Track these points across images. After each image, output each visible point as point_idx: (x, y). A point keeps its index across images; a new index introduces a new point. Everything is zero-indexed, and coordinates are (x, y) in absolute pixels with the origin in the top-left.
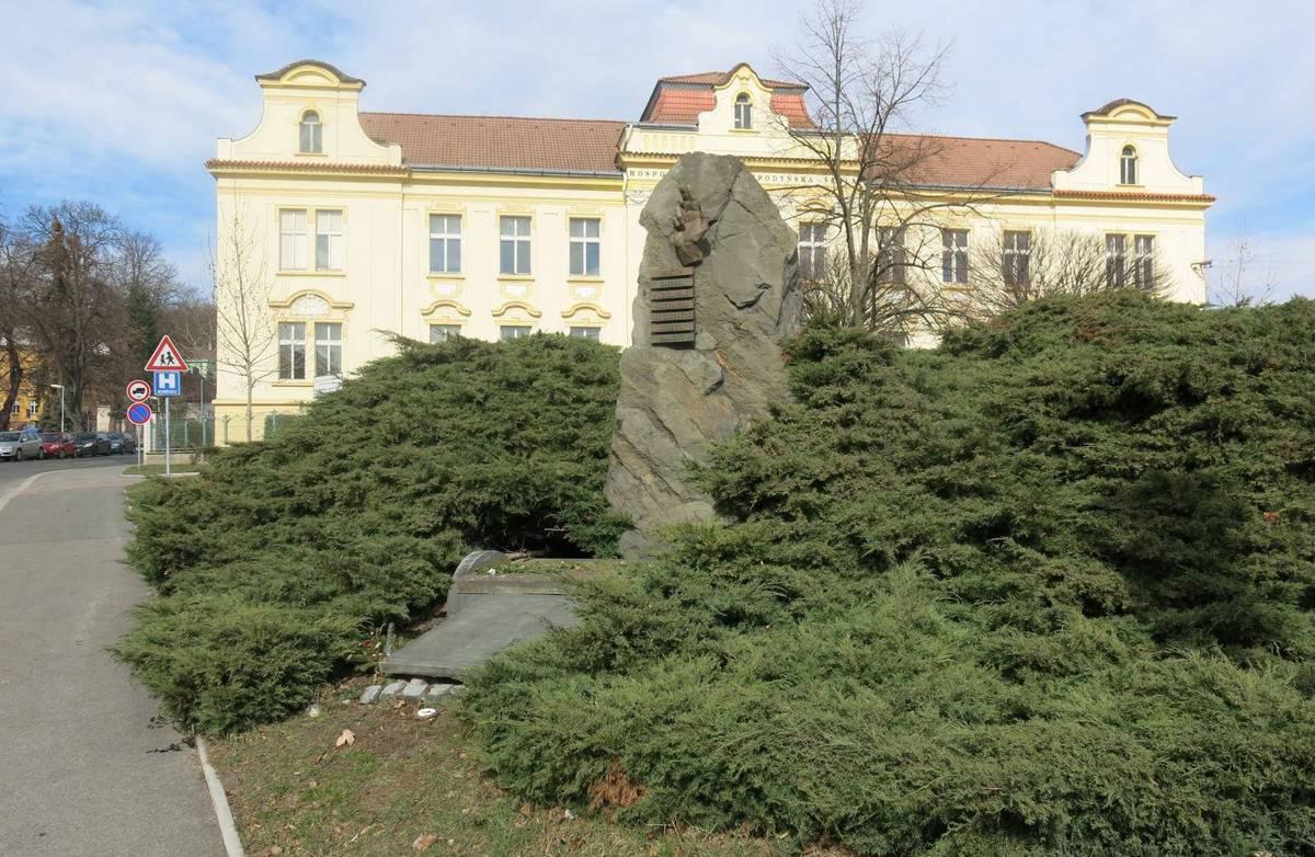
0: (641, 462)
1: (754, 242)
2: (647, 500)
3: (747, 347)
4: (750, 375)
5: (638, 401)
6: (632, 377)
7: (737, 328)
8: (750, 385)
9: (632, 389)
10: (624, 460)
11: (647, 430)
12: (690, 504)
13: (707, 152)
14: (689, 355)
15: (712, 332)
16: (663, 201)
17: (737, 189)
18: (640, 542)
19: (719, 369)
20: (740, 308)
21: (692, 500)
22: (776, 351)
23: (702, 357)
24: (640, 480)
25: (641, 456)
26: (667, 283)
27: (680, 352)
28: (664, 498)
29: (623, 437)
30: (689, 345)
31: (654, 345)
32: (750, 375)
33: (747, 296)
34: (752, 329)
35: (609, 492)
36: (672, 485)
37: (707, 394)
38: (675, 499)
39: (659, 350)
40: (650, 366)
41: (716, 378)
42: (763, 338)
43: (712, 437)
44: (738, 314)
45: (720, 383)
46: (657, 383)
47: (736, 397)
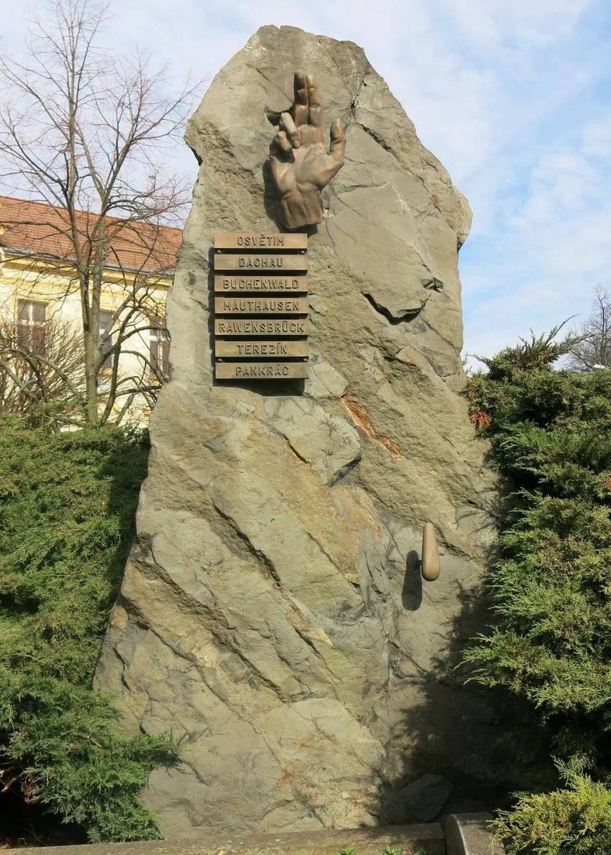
0: (192, 622)
1: (403, 204)
2: (204, 700)
3: (407, 394)
4: (412, 448)
5: (191, 495)
6: (177, 444)
7: (390, 359)
8: (411, 467)
9: (175, 469)
10: (154, 620)
11: (210, 554)
12: (300, 705)
13: (306, 31)
14: (292, 405)
15: (336, 363)
16: (236, 104)
17: (362, 105)
18: (194, 791)
19: (354, 435)
20: (394, 321)
21: (305, 696)
22: (460, 406)
23: (319, 410)
24: (191, 659)
25: (191, 607)
26: (250, 261)
27: (272, 401)
28: (243, 694)
29: (156, 571)
30: (293, 387)
31: (220, 382)
32: (412, 448)
33: (409, 298)
34: (420, 361)
35: (107, 684)
36: (262, 666)
37: (332, 484)
38: (266, 695)
39: (231, 394)
40: (218, 424)
41: (349, 453)
42: (435, 379)
43: (352, 568)
44: (393, 331)
45: (355, 463)
46: (232, 460)
47: (385, 491)
